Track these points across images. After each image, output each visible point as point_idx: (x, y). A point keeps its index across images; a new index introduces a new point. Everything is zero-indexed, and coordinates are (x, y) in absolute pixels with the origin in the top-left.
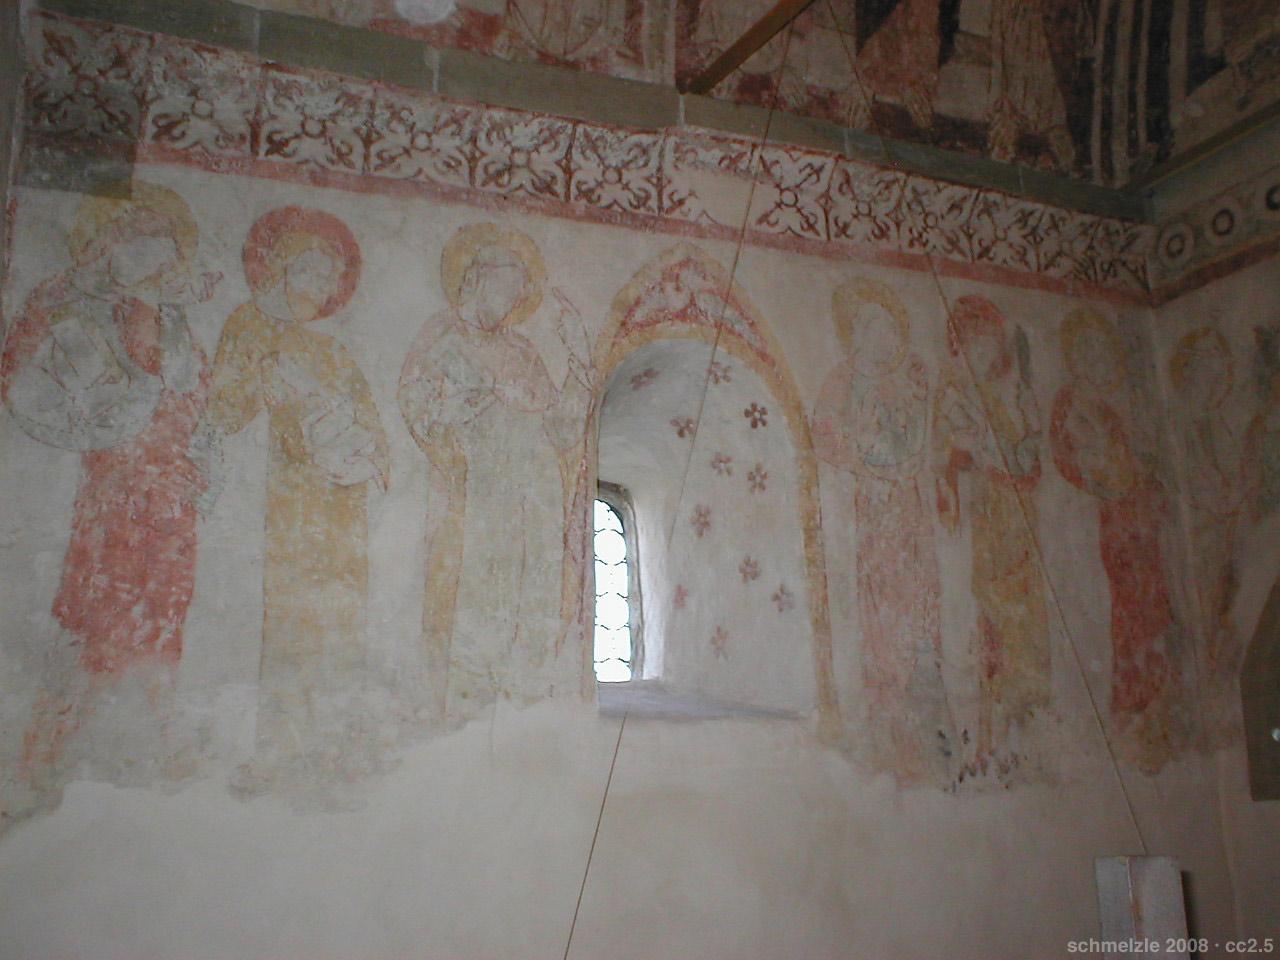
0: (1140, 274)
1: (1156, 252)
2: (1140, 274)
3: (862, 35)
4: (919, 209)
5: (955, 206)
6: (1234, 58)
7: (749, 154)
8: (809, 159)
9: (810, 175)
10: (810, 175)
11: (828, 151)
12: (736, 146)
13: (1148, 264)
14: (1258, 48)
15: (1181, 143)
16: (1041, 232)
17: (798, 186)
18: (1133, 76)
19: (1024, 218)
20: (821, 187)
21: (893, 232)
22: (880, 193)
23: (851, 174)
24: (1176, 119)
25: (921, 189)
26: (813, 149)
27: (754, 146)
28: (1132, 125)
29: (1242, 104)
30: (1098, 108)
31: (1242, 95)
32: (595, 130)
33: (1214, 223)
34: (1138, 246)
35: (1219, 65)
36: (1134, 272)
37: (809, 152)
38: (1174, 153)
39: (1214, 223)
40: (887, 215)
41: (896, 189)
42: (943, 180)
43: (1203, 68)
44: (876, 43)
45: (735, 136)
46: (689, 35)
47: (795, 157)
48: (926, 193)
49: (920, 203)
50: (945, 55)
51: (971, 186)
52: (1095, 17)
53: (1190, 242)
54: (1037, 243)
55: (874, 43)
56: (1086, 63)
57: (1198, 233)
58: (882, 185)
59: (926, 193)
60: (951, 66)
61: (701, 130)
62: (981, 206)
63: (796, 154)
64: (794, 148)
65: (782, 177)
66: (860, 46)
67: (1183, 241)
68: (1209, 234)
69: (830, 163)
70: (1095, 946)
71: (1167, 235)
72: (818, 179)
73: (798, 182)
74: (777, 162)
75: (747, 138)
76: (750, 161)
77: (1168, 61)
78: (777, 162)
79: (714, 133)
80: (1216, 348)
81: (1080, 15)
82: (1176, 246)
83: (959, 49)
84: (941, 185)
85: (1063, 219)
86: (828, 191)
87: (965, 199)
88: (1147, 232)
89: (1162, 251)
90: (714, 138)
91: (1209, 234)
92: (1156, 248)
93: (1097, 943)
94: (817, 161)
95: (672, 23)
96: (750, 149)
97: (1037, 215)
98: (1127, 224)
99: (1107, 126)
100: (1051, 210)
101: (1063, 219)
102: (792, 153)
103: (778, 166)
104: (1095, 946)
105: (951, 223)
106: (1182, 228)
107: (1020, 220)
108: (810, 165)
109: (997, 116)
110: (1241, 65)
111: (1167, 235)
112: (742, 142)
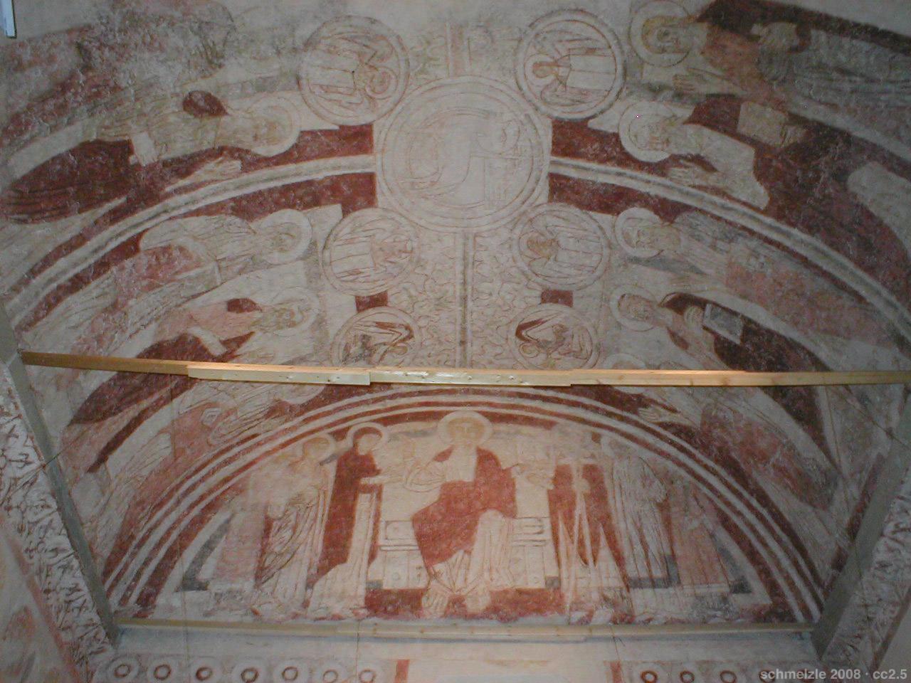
0: (90, 675)
1: (107, 668)
2: (90, 675)
3: (76, 420)
4: (42, 535)
5: (56, 551)
6: (215, 587)
7: (12, 418)
8: (31, 452)
9: (21, 461)
10: (21, 461)
11: (42, 457)
12: (12, 406)
13: (97, 673)
14: (230, 592)
15: (157, 614)
16: (74, 605)
17: (10, 461)
18: (146, 563)
19: (75, 589)
20: (19, 474)
21: (25, 534)
22: (37, 507)
23: (38, 481)
24: (161, 600)
25: (55, 524)
26: (39, 449)
27: (19, 416)
28: (130, 588)
29: (207, 614)
30: (121, 566)
31: (209, 609)
32: (777, 460)
33: (157, 669)
34: (101, 657)
35: (202, 587)
36: (88, 672)
37: (35, 449)
38: (150, 617)
39: (157, 669)
40: (29, 522)
41: (46, 511)
42: (68, 530)
43: (190, 583)
44: (78, 430)
45: (18, 400)
46: (22, 330)
47: (27, 444)
48: (54, 529)
49: (46, 532)
50: (92, 469)
51: (73, 546)
52: (150, 519)
53: (133, 674)
54: (67, 611)
55: (77, 429)
56: (132, 537)
57: (142, 670)
58: (42, 503)
59: (54, 529)
60: (90, 476)
61: (9, 380)
62: (65, 563)
63: (29, 443)
64: (32, 438)
65: (9, 448)
66: (72, 423)
67: (129, 670)
68: (150, 674)
69: (36, 464)
70: (780, 674)
71: (120, 662)
72: (22, 468)
73: (13, 459)
74: (17, 437)
75: (22, 408)
76: (9, 422)
77: (172, 568)
78: (17, 437)
79: (13, 388)
80: (878, 550)
81: (146, 511)
82: (122, 671)
83: (99, 473)
84: (64, 531)
85: (87, 609)
86: (19, 479)
87: (64, 550)
88: (110, 652)
89: (111, 669)
90: (10, 391)
91: (150, 674)
92: (108, 666)
93: (782, 673)
94: (33, 456)
95: (24, 314)
96: (15, 415)
97: (80, 594)
98: (107, 640)
99: (117, 579)
100: (88, 597)
101: (87, 609)
102: (29, 439)
103: (15, 439)
104: (780, 674)
105: (48, 558)
106: (133, 662)
107: (70, 589)
108: (27, 455)
109: (89, 524)
110: (216, 594)
111: (120, 662)
112: (17, 407)
